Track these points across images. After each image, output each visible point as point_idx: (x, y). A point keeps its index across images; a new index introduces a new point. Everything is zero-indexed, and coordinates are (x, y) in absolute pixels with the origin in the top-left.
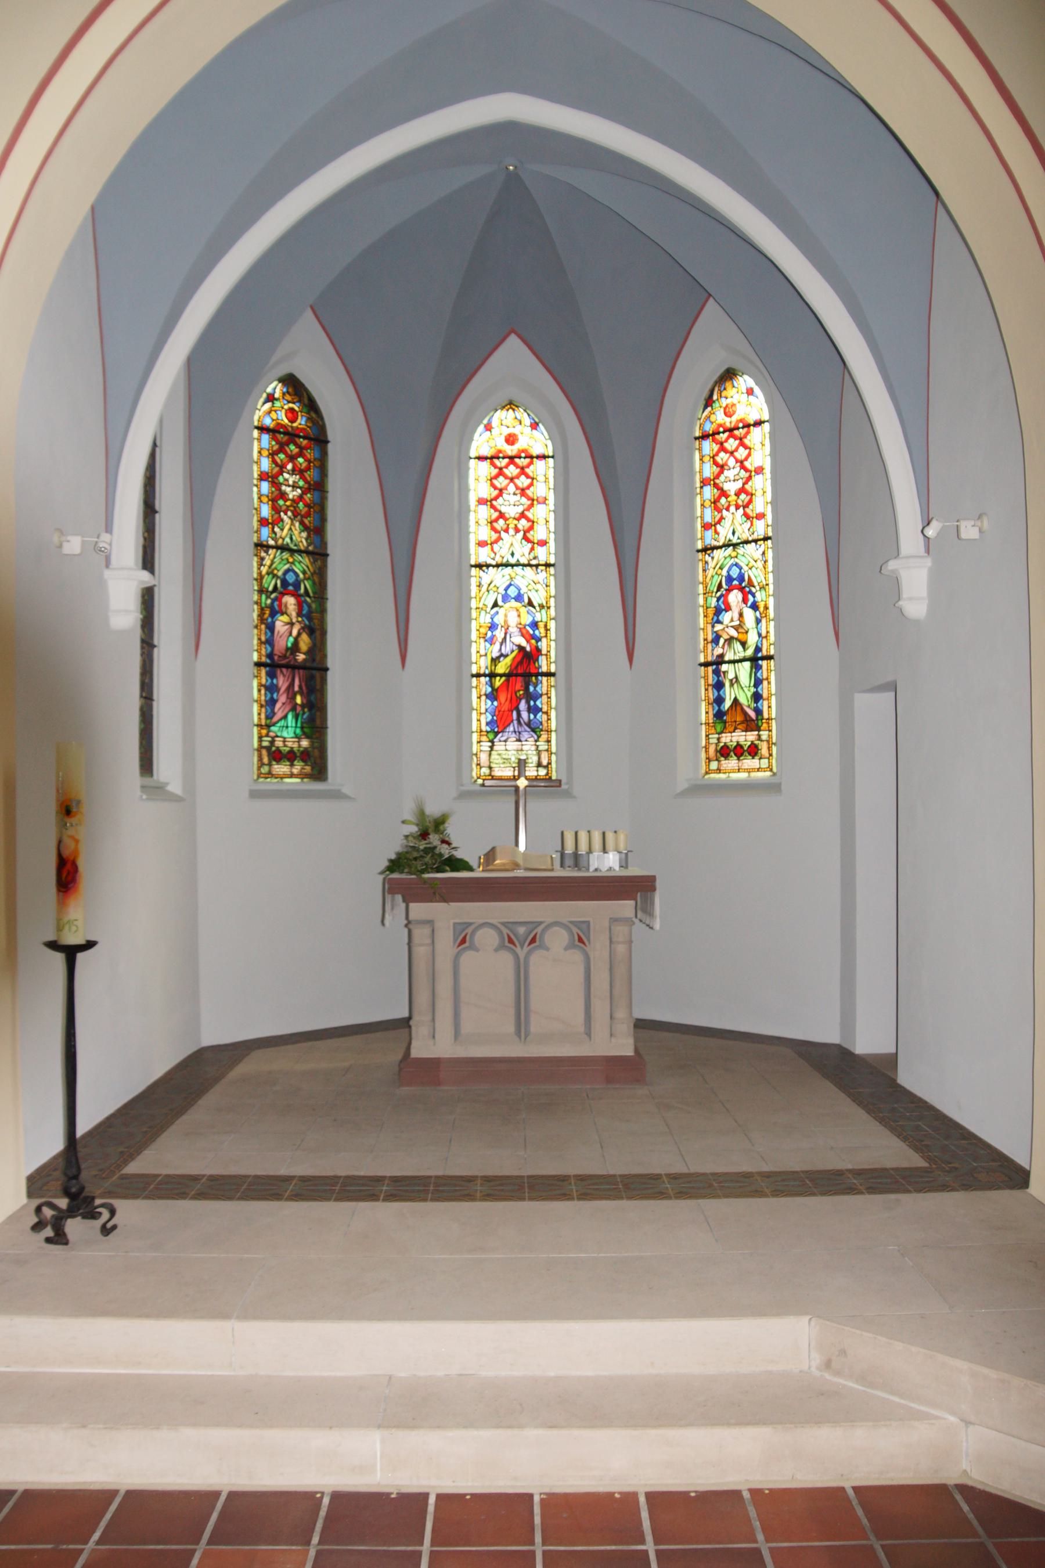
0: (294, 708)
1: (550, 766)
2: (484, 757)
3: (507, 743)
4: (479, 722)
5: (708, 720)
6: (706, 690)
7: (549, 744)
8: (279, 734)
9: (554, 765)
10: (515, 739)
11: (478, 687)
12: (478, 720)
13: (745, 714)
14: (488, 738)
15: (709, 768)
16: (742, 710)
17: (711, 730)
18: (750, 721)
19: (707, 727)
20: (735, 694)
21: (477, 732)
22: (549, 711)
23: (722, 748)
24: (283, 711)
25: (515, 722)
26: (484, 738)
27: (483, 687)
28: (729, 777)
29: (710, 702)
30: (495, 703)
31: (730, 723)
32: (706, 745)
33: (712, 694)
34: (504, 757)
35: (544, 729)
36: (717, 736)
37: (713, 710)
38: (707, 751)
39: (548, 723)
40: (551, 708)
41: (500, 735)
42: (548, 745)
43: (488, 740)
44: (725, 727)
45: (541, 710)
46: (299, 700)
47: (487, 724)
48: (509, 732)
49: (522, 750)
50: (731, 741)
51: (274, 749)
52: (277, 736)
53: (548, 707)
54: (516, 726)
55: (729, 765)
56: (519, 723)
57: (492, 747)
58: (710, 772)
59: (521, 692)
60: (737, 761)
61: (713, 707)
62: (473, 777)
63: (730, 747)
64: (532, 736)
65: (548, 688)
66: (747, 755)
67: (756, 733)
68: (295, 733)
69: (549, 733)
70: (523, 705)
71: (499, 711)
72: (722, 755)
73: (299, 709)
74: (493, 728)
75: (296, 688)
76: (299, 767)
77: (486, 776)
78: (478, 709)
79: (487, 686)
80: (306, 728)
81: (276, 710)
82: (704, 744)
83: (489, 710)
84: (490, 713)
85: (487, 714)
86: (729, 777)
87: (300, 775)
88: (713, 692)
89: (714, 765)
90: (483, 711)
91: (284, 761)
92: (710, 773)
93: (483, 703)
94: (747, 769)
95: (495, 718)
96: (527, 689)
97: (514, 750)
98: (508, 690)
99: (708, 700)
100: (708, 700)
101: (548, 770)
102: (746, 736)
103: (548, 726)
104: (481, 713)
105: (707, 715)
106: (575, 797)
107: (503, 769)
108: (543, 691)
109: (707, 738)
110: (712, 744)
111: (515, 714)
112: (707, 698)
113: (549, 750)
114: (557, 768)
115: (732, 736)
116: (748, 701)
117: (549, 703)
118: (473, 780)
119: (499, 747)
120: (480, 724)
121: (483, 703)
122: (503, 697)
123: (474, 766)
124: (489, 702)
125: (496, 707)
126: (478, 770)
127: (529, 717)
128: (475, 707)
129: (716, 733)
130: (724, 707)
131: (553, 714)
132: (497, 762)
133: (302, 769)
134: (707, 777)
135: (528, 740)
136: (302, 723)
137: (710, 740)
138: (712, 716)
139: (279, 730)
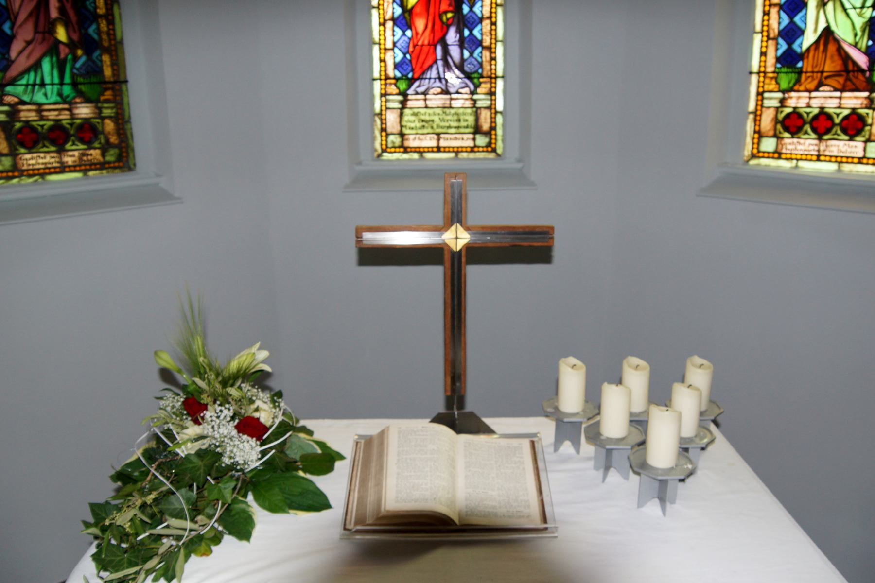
0: (54, 48)
1: (493, 132)
2: (392, 118)
3: (428, 97)
4: (383, 64)
5: (765, 67)
6: (766, 13)
7: (493, 97)
8: (26, 98)
9: (499, 131)
10: (439, 90)
11: (381, 7)
12: (381, 61)
13: (846, 58)
14: (398, 88)
15: (758, 148)
16: (840, 49)
17: (770, 84)
18: (853, 71)
19: (762, 79)
20: (827, 21)
21: (381, 79)
22: (493, 46)
23: (788, 116)
24: (28, 57)
25: (440, 63)
26: (392, 89)
27: (388, 6)
28: (797, 167)
29: (772, 36)
30: (409, 33)
31: (808, 74)
32: (756, 110)
33: (778, 21)
34: (423, 117)
35: (485, 74)
36: (780, 95)
37: (777, 49)
38: (757, 120)
39: (491, 65)
40: (496, 41)
41: (417, 83)
42: (491, 100)
43: (397, 91)
44: (798, 81)
45: (480, 43)
46: (61, 34)
47: (396, 66)
48: (430, 79)
49: (451, 107)
50: (809, 106)
51: (18, 125)
52: (23, 103)
53: (491, 39)
54: (441, 69)
55: (799, 147)
56: (447, 65)
57: (404, 104)
58: (761, 155)
59: (450, 15)
60: (816, 142)
61: (777, 44)
62: (376, 150)
63: (805, 115)
64: (467, 86)
65: (491, 8)
66: (839, 132)
67: (866, 94)
68: (60, 94)
69: (493, 80)
70: (452, 36)
71: (415, 46)
72: (787, 129)
73: (64, 51)
74: (405, 73)
75: (54, 14)
76: (76, 153)
77: (395, 148)
78: (382, 42)
79: (395, 5)
80: (84, 84)
81: (13, 54)
82: (752, 107)
83: (398, 45)
84: (400, 50)
85: (396, 50)
86: (797, 167)
87: (80, 166)
88: (780, 18)
89: (769, 145)
90: (389, 45)
91: (44, 146)
92: (759, 157)
93: (389, 33)
94: (836, 157)
95: (408, 56)
96: (458, 10)
97: (438, 107)
98: (428, 11)
99: (768, 31)
100: (768, 31)
101: (491, 139)
102: (840, 98)
103: (491, 69)
104: (385, 49)
105: (763, 58)
106: (533, 184)
107: (422, 137)
108: (484, 12)
109: (760, 97)
110: (769, 108)
111: (439, 49)
112: (766, 25)
113: (493, 107)
114: (504, 135)
115: (810, 98)
116: (856, 35)
117: (493, 32)
118: (376, 154)
119: (416, 102)
120: (385, 66)
121: (389, 33)
122: (420, 24)
123: (377, 133)
124: (398, 32)
125: (410, 39)
126: (384, 138)
127: (462, 54)
128: (377, 39)
129: (779, 91)
130: (800, 46)
131: (500, 49)
132: (412, 125)
133: (83, 155)
134: (753, 162)
135: (461, 91)
136: (73, 76)
137: (765, 101)
138: (774, 61)
139: (25, 91)
